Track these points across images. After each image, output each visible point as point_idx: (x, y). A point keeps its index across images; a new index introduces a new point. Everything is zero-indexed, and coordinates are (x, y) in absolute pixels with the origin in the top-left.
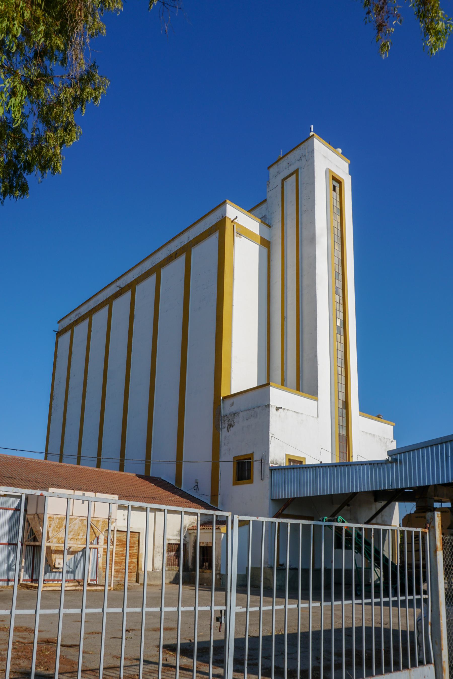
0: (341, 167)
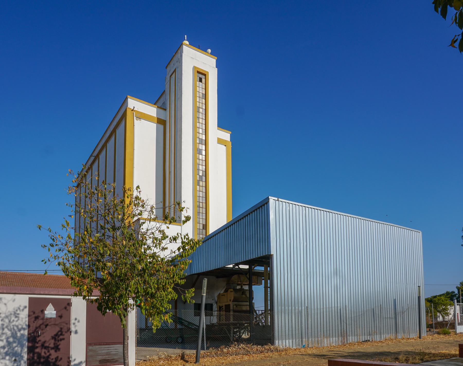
0: (208, 63)
